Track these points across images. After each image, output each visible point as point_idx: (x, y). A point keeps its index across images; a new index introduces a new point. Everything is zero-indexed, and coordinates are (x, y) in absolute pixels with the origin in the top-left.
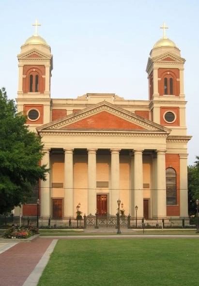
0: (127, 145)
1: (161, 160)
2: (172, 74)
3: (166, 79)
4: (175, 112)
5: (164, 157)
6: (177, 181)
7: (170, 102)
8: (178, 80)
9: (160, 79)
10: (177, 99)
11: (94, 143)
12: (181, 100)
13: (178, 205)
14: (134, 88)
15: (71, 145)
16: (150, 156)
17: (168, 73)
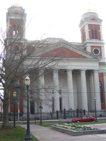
0: (91, 67)
1: (96, 76)
2: (96, 28)
3: (93, 30)
4: (99, 49)
5: (98, 74)
6: (103, 89)
7: (96, 43)
8: (99, 31)
9: (90, 30)
10: (99, 41)
11: (82, 66)
12: (102, 42)
13: (104, 103)
14: (73, 36)
15: (86, 67)
16: (89, 73)
17: (94, 27)
